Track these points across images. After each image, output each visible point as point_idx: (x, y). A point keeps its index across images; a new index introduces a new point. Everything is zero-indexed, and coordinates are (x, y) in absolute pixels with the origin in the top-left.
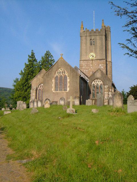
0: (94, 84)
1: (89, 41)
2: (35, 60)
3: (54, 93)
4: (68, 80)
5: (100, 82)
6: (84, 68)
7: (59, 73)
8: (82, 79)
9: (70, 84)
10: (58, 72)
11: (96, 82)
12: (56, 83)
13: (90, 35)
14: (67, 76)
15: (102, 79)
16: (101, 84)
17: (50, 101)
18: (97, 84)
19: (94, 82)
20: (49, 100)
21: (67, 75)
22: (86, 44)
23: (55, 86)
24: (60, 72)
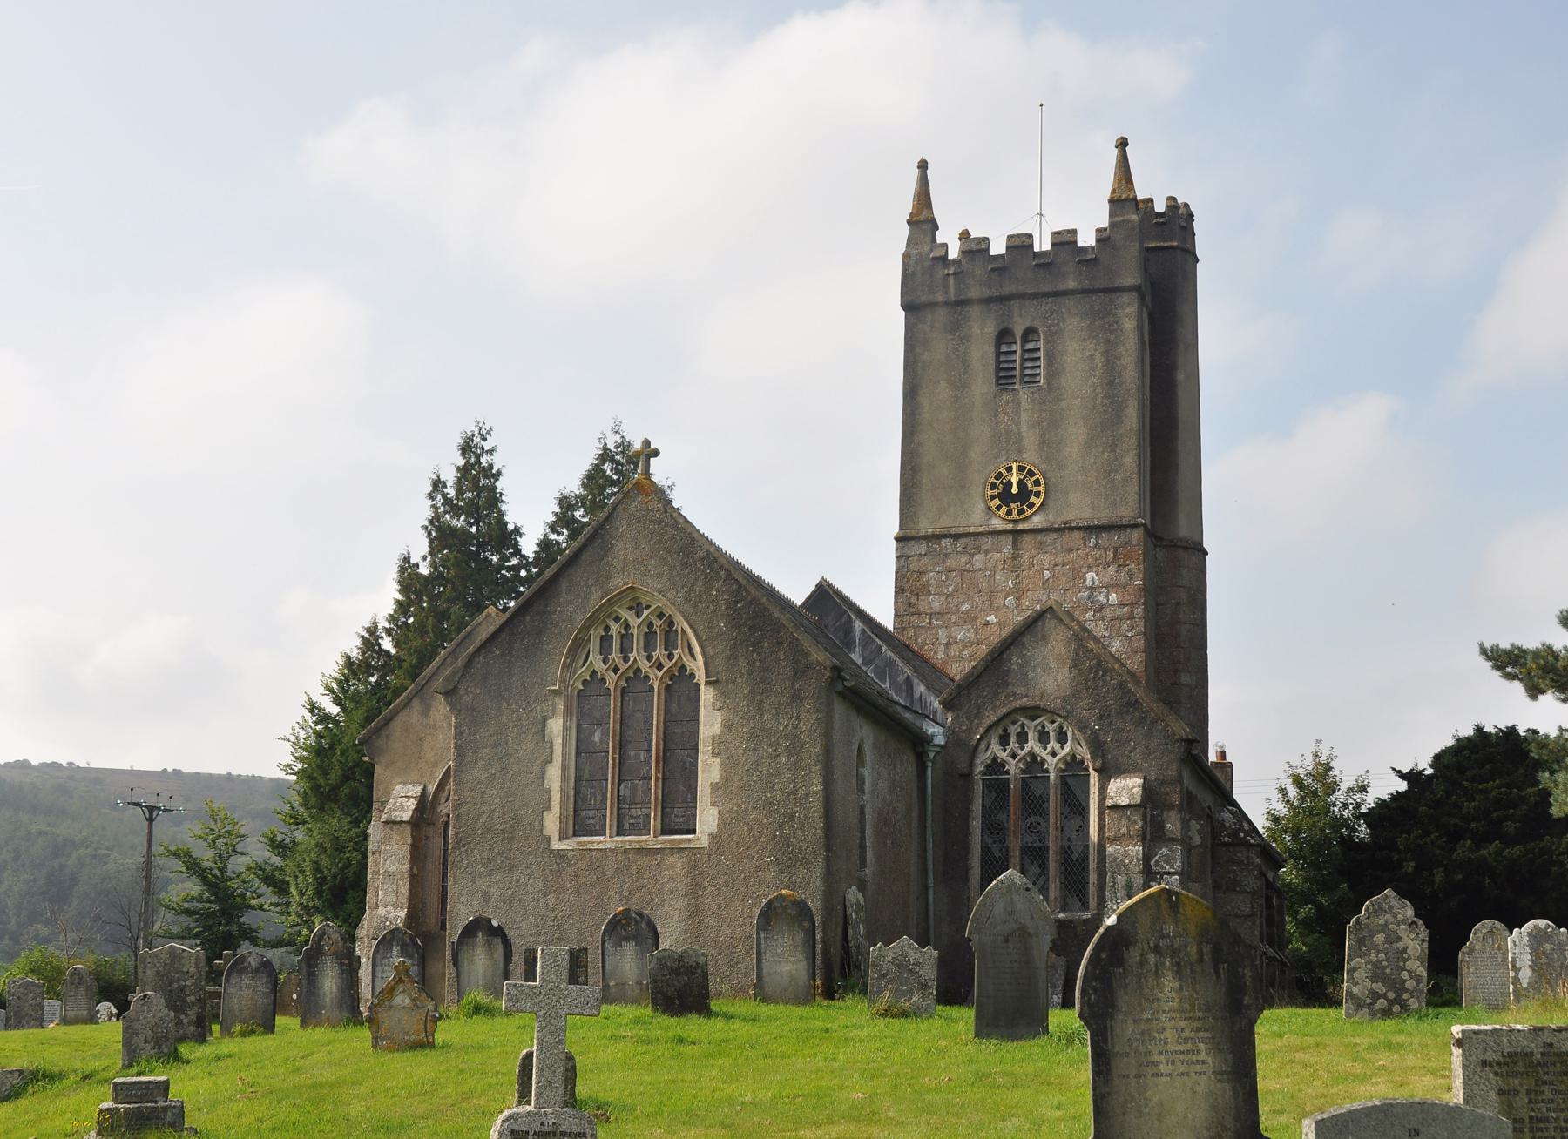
0: (996, 766)
1: (990, 350)
2: (506, 538)
3: (560, 855)
4: (710, 723)
5: (1062, 738)
6: (936, 603)
7: (616, 644)
8: (860, 710)
9: (729, 767)
10: (606, 640)
11: (1022, 737)
12: (583, 749)
13: (995, 292)
14: (701, 677)
15: (1083, 708)
16: (1073, 765)
17: (507, 944)
18: (1034, 762)
19: (1004, 741)
20: (499, 932)
21: (698, 666)
22: (960, 386)
23: (578, 780)
24: (626, 637)
